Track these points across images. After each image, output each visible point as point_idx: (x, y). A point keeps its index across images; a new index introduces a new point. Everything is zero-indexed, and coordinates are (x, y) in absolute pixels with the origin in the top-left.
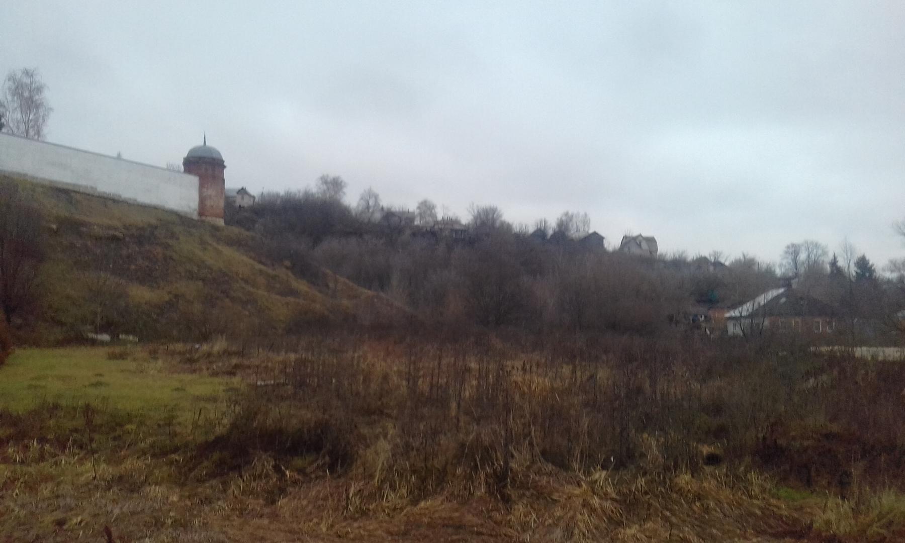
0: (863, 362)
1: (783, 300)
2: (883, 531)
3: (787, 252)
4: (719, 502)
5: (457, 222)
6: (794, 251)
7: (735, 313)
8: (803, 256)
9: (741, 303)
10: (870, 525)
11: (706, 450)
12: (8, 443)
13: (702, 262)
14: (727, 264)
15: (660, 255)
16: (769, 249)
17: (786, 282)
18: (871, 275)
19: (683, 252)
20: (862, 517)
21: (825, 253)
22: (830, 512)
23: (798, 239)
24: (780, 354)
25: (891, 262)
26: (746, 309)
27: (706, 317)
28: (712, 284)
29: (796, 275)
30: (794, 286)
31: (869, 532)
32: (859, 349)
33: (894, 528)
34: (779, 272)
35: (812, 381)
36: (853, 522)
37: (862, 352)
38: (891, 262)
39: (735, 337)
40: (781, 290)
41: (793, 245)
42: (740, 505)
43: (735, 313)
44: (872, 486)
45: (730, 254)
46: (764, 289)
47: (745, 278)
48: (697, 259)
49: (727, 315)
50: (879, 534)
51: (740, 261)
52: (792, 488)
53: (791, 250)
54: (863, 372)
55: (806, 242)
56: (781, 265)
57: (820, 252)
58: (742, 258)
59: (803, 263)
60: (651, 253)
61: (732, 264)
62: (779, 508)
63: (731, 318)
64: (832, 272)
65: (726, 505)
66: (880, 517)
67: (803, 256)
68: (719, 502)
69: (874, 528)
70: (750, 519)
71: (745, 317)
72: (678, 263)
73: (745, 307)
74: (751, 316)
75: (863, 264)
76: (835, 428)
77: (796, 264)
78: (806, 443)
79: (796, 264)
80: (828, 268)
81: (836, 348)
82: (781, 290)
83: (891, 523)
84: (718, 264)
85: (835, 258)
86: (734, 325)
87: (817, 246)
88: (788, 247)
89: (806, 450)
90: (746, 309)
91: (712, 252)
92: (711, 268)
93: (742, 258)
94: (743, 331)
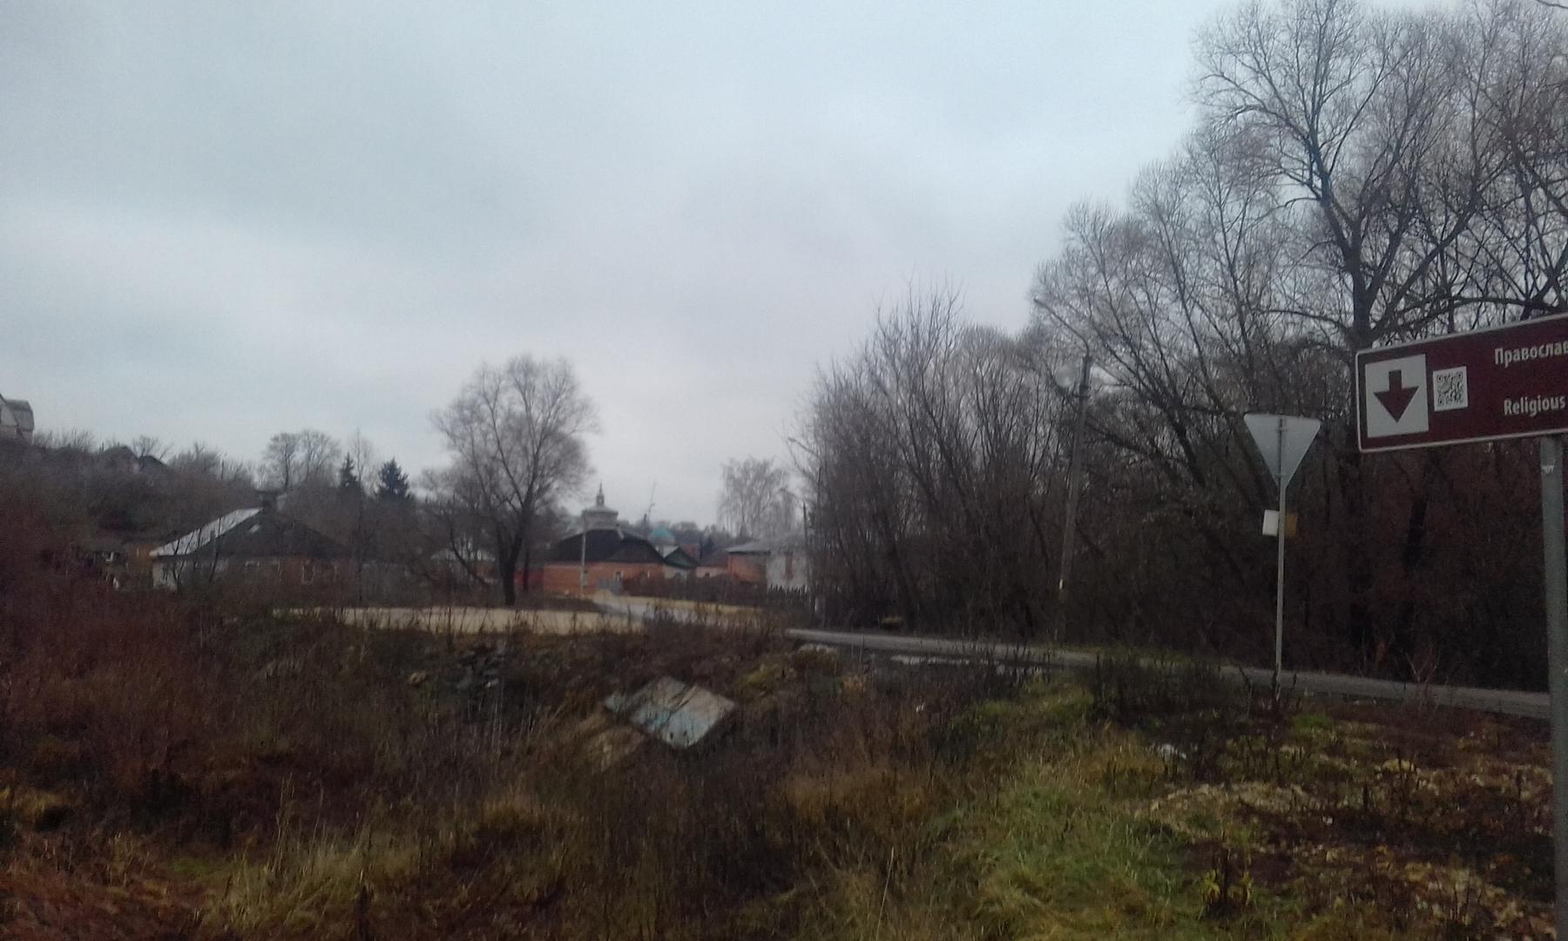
0: (355, 629)
1: (255, 528)
2: (311, 915)
3: (272, 448)
4: (34, 899)
5: (250, 479)
6: (285, 445)
7: (167, 550)
8: (299, 456)
9: (177, 534)
10: (292, 908)
11: (42, 802)
12: (729, 696)
13: (120, 454)
14: (165, 460)
15: (39, 437)
16: (243, 442)
17: (266, 498)
18: (402, 494)
19: (85, 435)
20: (281, 895)
21: (335, 453)
22: (238, 891)
23: (293, 429)
24: (226, 622)
25: (425, 473)
26: (187, 544)
27: (117, 555)
28: (137, 495)
29: (287, 486)
30: (280, 506)
31: (290, 919)
32: (351, 611)
33: (327, 906)
34: (258, 481)
35: (270, 667)
36: (266, 905)
37: (351, 615)
38: (425, 473)
39: (163, 590)
40: (254, 512)
41: (285, 436)
42: (77, 899)
43: (167, 550)
44: (305, 839)
45: (173, 439)
46: (220, 508)
47: (194, 488)
48: (111, 451)
49: (153, 553)
50: (303, 920)
51: (189, 457)
52: (196, 856)
53: (282, 444)
54: (352, 648)
55: (306, 433)
56: (261, 469)
57: (327, 451)
58: (193, 451)
59: (298, 468)
60: (19, 431)
61: (174, 461)
62: (157, 895)
63: (160, 558)
64: (343, 484)
65: (46, 904)
66: (310, 890)
67: (299, 456)
68: (34, 899)
69: (299, 913)
70: (91, 923)
71: (184, 557)
72: (72, 456)
73: (185, 540)
74: (195, 556)
75: (391, 474)
76: (283, 745)
77: (287, 469)
78: (231, 775)
79: (287, 469)
80: (337, 478)
81: (318, 610)
82: (254, 512)
83: (324, 899)
84: (149, 461)
85: (349, 462)
86: (166, 571)
87: (323, 440)
88: (276, 439)
89: (226, 787)
90: (187, 544)
91: (138, 439)
92: (136, 467)
93: (193, 451)
94: (178, 583)
